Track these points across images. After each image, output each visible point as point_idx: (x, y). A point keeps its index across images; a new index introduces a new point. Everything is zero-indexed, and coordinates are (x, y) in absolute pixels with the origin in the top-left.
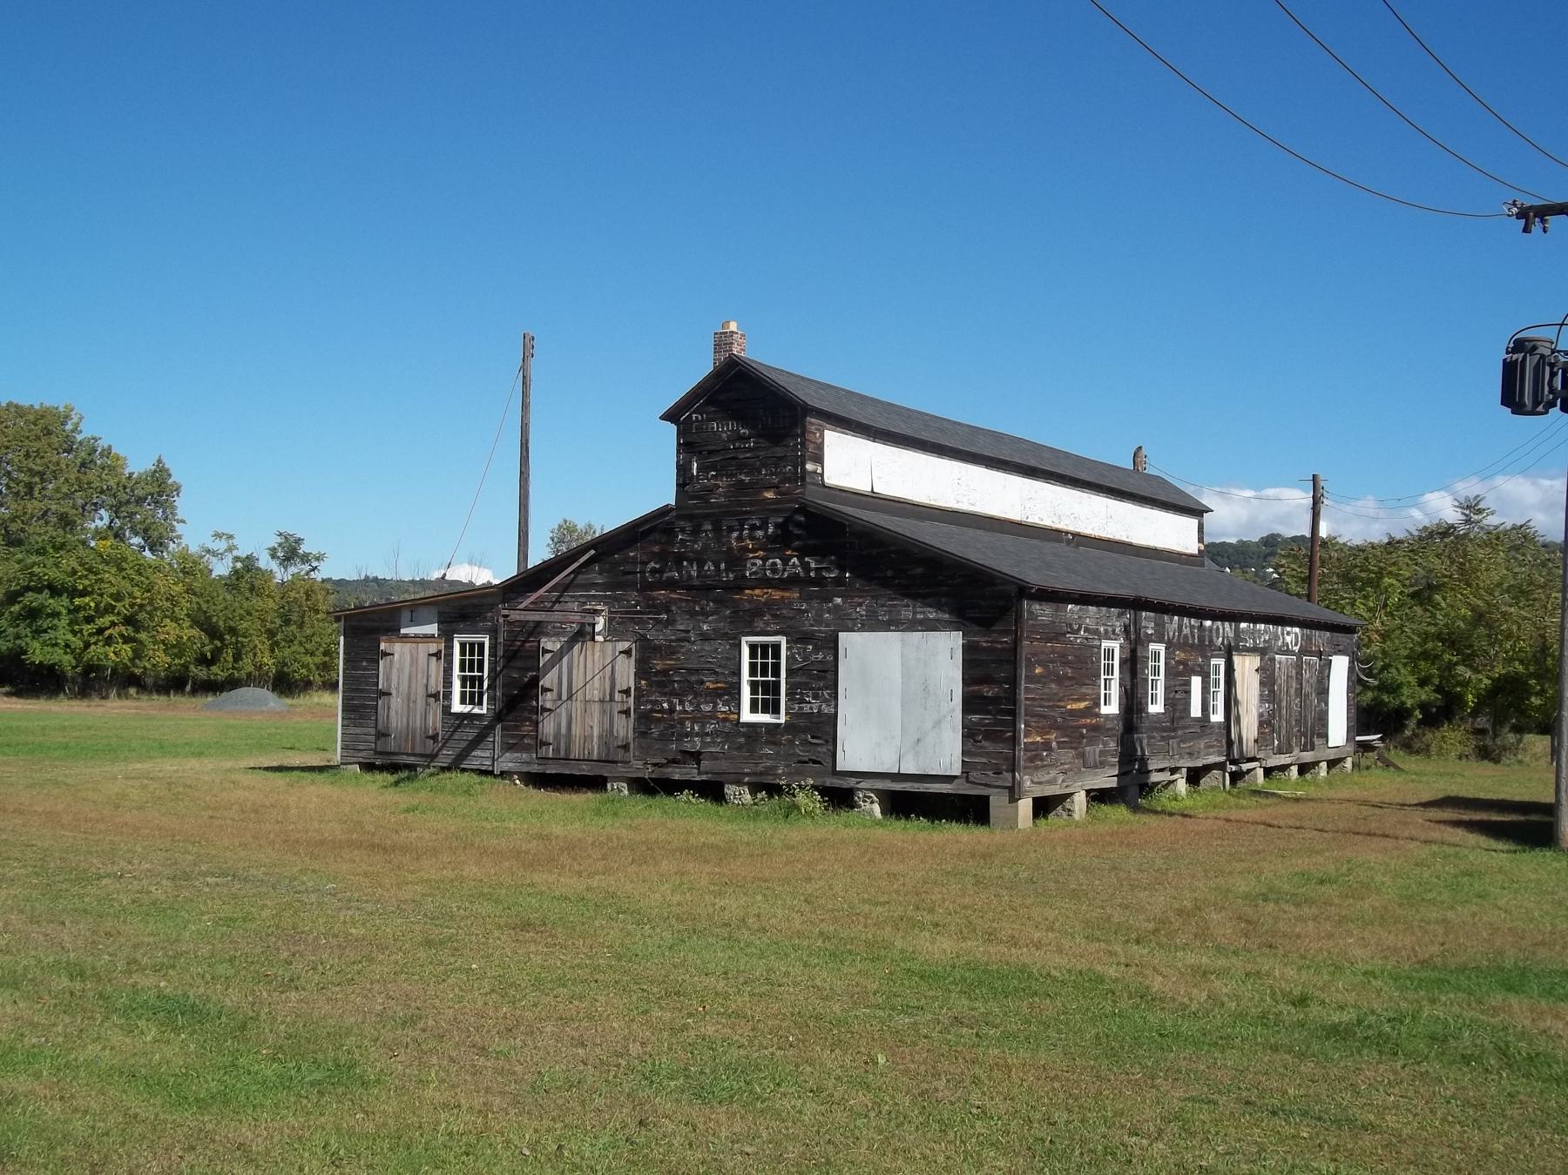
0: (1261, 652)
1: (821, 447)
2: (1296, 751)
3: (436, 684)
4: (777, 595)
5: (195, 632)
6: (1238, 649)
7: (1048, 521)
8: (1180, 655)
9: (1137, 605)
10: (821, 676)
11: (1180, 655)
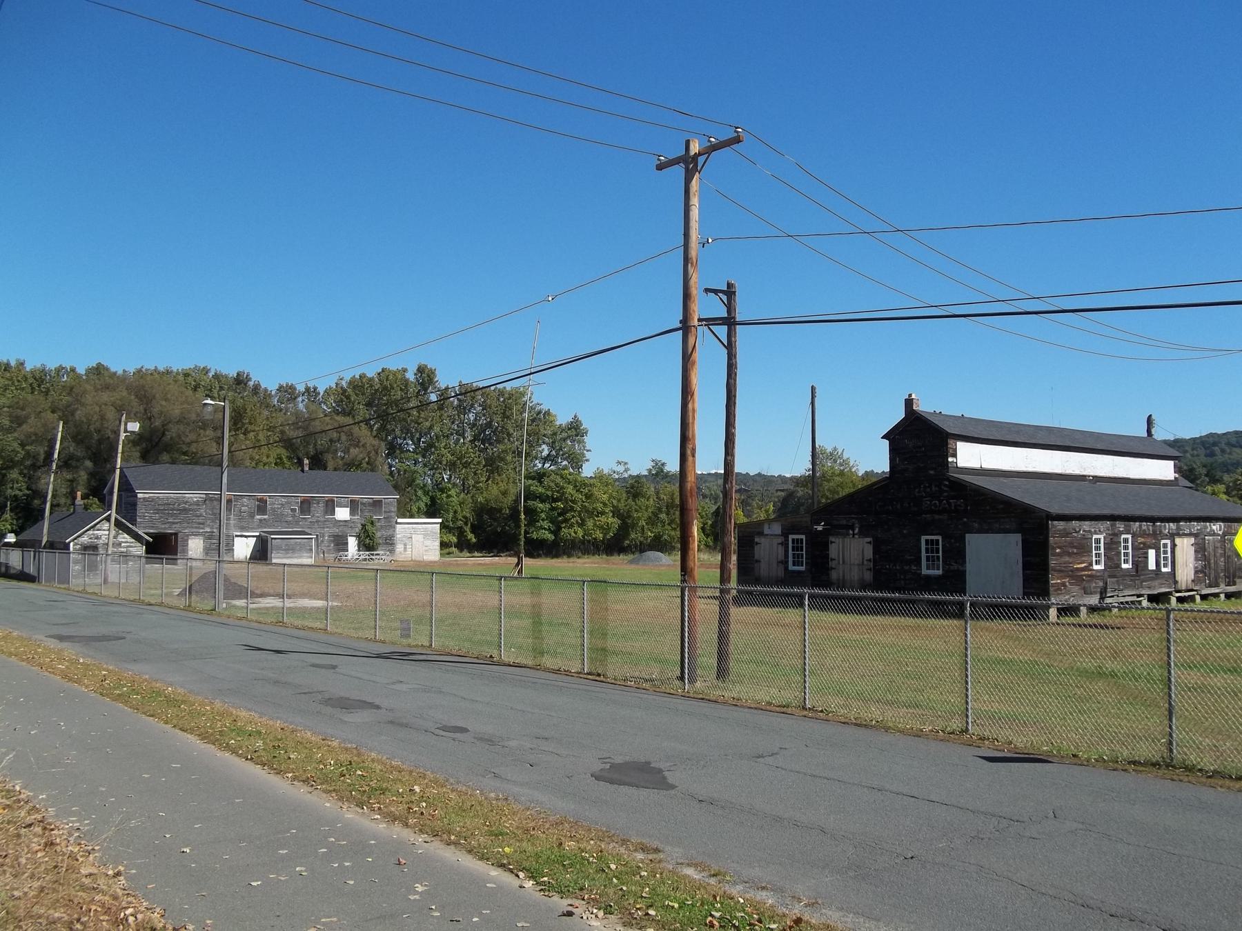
0: (1196, 536)
1: (955, 450)
2: (1222, 586)
3: (781, 557)
4: (937, 517)
5: (616, 520)
6: (1179, 535)
7: (1077, 472)
8: (1140, 540)
9: (1113, 518)
10: (956, 554)
11: (1140, 540)
